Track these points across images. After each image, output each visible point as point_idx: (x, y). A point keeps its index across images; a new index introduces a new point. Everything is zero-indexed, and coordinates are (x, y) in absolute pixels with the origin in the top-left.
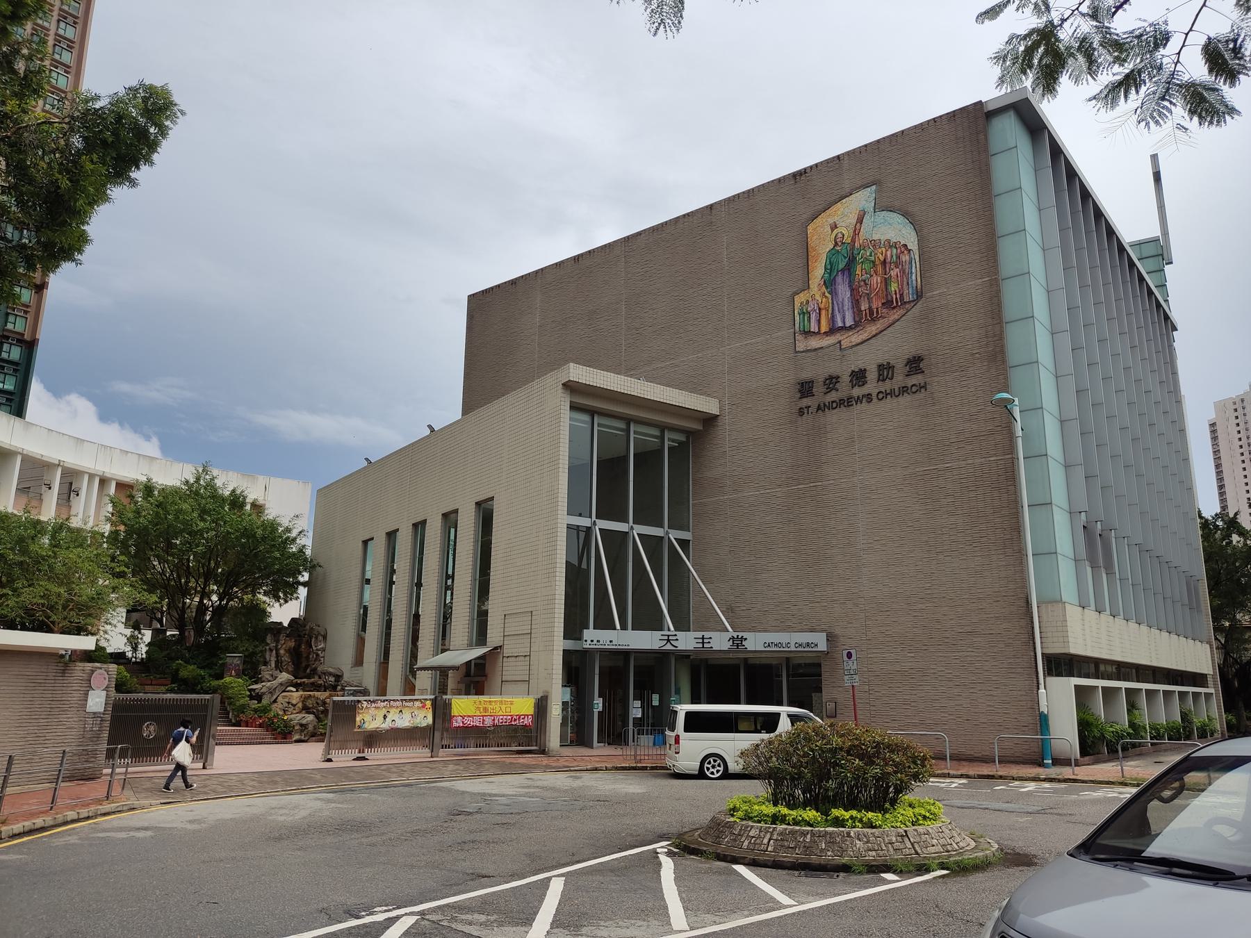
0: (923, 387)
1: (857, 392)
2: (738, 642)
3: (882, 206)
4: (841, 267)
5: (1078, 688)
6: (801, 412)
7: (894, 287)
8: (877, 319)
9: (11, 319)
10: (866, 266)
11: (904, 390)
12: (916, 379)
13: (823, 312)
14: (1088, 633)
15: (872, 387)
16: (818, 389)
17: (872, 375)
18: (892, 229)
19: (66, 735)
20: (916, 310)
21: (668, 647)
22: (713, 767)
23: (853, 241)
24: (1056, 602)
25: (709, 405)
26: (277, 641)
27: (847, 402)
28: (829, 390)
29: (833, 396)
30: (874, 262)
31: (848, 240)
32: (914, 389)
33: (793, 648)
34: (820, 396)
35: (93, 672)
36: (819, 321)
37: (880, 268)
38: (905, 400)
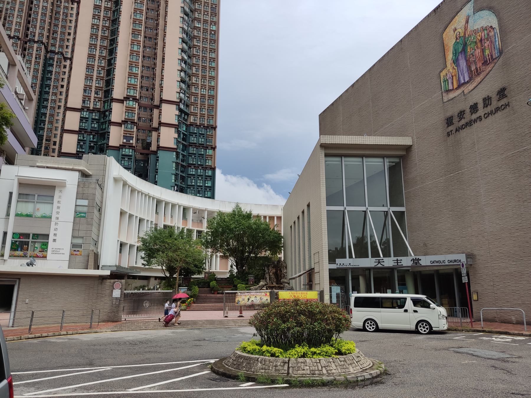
0: (507, 105)
1: (474, 116)
2: (416, 261)
3: (477, 10)
4: (460, 50)
6: (448, 135)
7: (487, 52)
9: (207, 161)
10: (472, 46)
11: (497, 109)
12: (504, 101)
13: (454, 78)
15: (481, 112)
17: (480, 106)
18: (487, 19)
19: (104, 307)
20: (500, 62)
21: (379, 265)
22: (424, 327)
23: (465, 34)
25: (406, 141)
26: (268, 270)
27: (469, 124)
28: (461, 119)
29: (463, 122)
30: (476, 42)
32: (503, 107)
33: (447, 263)
34: (457, 124)
35: (114, 283)
36: (453, 83)
37: (479, 44)
38: (499, 113)
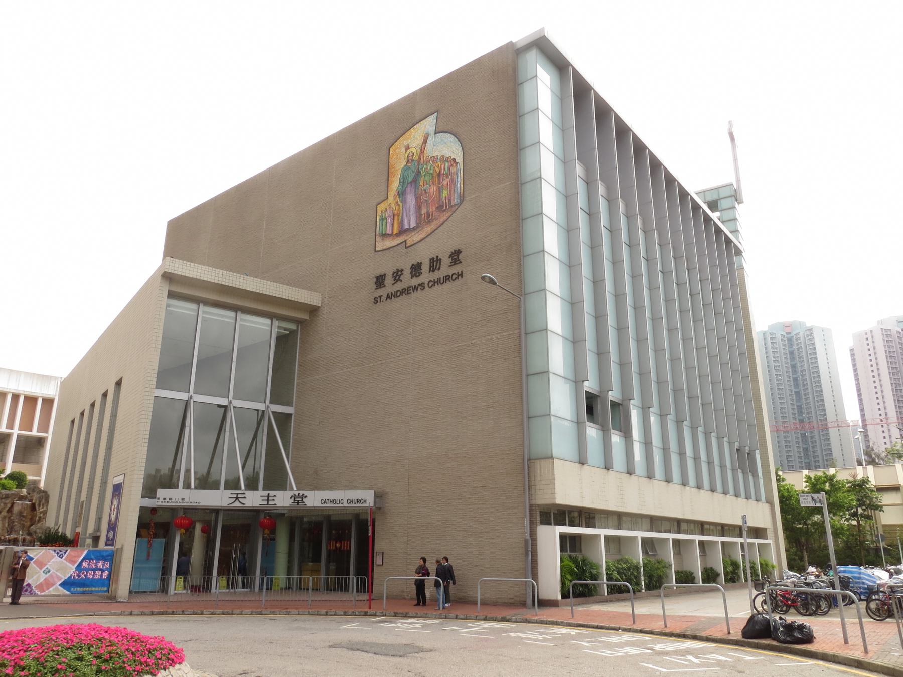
0: (460, 275)
1: (415, 282)
2: (299, 499)
4: (410, 180)
5: (563, 537)
6: (376, 301)
7: (445, 193)
8: (432, 220)
10: (427, 178)
11: (447, 278)
12: (457, 269)
13: (396, 217)
14: (571, 486)
15: (426, 276)
16: (389, 281)
17: (426, 267)
18: (448, 148)
21: (237, 504)
23: (420, 159)
24: (548, 458)
29: (399, 286)
31: (416, 158)
33: (346, 505)
34: (390, 287)
36: (393, 225)
37: (436, 179)
38: (449, 285)
